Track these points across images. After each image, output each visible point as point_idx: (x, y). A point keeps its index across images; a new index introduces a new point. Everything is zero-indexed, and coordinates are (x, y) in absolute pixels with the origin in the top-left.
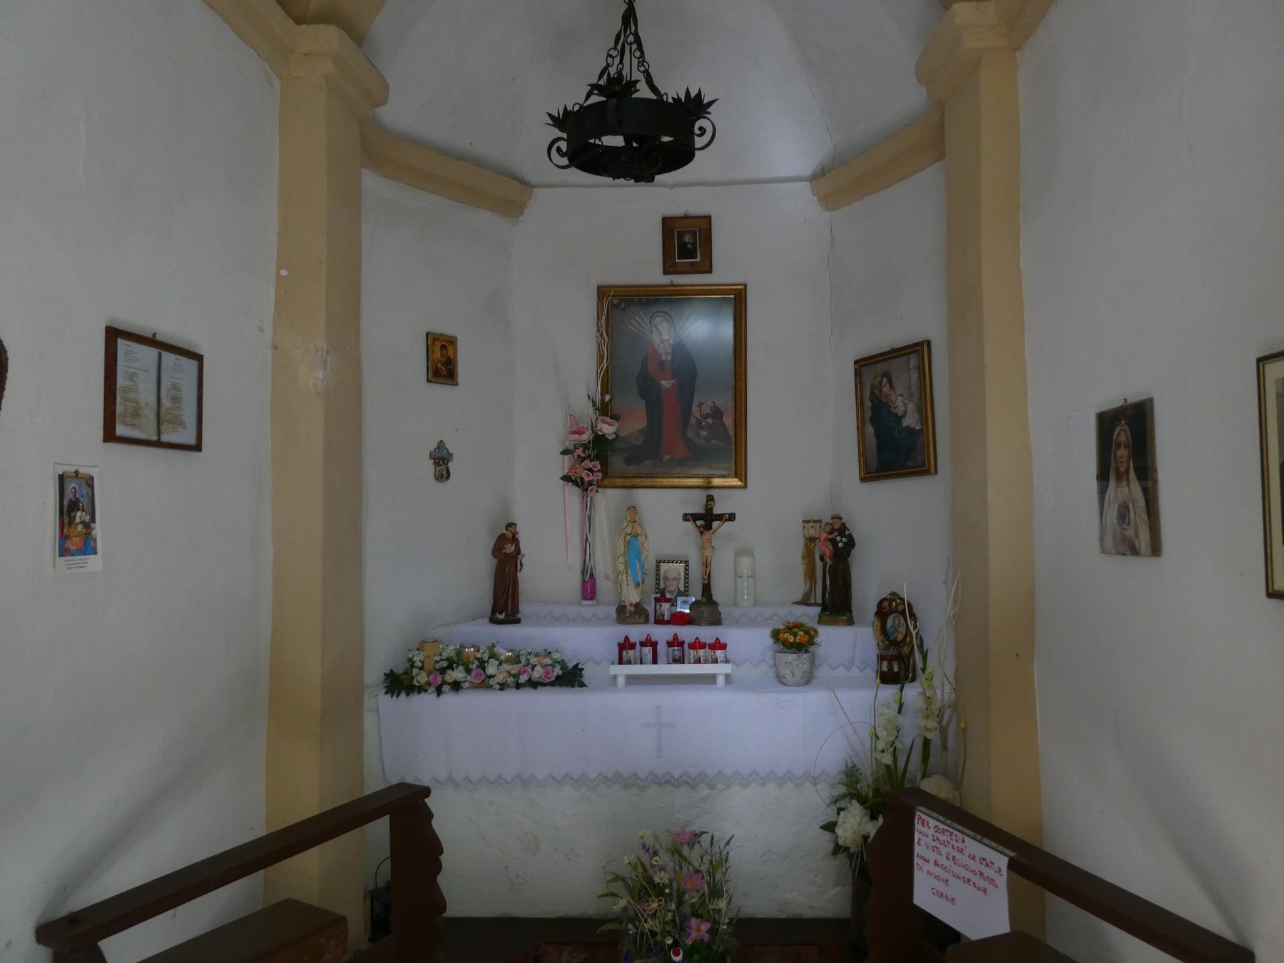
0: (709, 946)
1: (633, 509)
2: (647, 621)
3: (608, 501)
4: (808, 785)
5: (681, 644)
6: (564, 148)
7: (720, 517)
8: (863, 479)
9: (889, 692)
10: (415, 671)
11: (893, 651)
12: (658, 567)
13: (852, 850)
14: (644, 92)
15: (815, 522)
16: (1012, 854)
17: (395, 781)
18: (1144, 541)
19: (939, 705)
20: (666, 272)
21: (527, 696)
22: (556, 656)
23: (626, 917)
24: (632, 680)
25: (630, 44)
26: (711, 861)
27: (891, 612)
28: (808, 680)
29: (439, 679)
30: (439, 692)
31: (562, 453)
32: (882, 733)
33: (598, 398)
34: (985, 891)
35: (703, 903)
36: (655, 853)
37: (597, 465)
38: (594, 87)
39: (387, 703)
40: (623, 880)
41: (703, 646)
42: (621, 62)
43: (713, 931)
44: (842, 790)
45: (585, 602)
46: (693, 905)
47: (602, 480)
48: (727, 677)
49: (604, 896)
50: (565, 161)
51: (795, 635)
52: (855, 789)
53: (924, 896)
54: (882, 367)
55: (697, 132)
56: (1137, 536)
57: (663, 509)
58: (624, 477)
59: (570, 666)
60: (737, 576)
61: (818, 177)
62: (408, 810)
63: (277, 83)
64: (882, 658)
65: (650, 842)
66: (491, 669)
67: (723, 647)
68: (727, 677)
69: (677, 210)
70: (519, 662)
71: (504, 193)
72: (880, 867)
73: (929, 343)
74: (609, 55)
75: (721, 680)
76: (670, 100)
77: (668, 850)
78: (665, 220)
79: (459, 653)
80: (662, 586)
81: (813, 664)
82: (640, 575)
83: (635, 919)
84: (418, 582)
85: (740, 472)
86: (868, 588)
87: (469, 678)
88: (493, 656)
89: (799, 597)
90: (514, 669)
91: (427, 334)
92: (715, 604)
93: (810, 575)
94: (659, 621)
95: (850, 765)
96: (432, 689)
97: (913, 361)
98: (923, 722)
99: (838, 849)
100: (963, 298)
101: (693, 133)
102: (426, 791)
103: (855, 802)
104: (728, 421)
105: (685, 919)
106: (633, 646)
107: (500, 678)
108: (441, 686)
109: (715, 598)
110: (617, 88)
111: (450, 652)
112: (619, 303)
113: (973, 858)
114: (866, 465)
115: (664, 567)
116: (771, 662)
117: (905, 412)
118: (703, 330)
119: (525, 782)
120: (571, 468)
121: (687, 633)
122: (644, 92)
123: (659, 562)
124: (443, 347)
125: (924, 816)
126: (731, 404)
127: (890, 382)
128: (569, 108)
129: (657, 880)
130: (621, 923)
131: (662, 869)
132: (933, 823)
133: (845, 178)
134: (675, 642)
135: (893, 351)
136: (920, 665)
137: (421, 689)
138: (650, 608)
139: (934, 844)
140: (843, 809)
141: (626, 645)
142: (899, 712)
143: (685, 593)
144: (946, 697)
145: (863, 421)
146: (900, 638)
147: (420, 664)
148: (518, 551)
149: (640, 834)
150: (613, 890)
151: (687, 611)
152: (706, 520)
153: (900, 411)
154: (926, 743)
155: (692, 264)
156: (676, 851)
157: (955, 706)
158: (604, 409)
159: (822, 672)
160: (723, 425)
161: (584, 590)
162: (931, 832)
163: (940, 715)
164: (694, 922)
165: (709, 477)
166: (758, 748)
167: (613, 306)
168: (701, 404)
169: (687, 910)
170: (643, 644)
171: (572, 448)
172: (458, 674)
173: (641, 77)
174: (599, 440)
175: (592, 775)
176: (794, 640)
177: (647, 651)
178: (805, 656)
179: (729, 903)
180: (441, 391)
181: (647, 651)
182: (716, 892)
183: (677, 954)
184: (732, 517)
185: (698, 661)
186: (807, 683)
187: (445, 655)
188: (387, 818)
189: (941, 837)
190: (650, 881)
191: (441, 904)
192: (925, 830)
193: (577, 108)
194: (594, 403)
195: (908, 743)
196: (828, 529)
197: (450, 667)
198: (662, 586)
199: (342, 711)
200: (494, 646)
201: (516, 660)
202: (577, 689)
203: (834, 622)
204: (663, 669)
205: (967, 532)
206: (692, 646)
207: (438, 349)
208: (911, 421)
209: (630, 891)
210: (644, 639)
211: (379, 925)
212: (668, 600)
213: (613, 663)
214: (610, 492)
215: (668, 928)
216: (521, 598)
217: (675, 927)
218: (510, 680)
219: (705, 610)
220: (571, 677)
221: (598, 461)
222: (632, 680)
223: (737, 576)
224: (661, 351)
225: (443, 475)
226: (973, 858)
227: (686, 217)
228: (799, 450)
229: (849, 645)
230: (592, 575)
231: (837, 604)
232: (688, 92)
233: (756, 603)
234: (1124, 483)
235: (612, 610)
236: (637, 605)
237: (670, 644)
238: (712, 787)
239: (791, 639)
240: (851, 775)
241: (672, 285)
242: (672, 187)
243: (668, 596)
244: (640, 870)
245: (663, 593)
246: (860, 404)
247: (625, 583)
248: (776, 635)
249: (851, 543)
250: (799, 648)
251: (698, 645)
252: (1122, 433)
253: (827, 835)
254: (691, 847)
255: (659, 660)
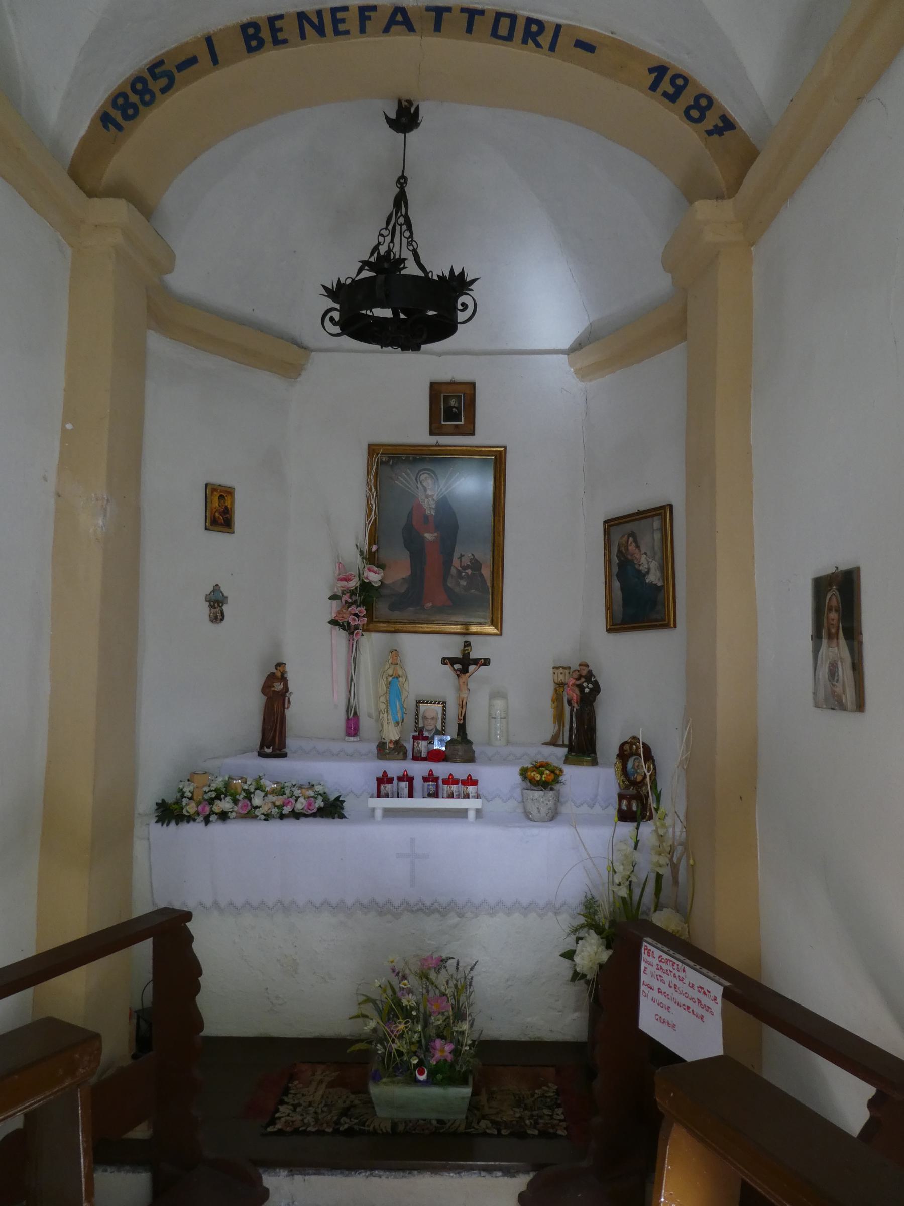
0: (452, 1066)
1: (395, 652)
2: (405, 758)
3: (372, 644)
4: (551, 914)
5: (436, 780)
6: (337, 318)
7: (476, 662)
8: (609, 630)
9: (627, 829)
10: (185, 801)
11: (632, 791)
12: (418, 706)
13: (588, 977)
14: (411, 269)
15: (564, 668)
16: (727, 984)
17: (162, 905)
18: (849, 697)
19: (670, 843)
20: (432, 433)
21: (290, 827)
22: (318, 788)
23: (377, 1037)
24: (389, 813)
25: (401, 225)
26: (456, 986)
27: (631, 755)
28: (553, 816)
29: (208, 809)
30: (207, 821)
31: (330, 599)
32: (619, 868)
33: (365, 549)
34: (702, 1018)
35: (447, 1025)
36: (404, 977)
37: (363, 609)
38: (365, 264)
39: (158, 831)
40: (374, 1002)
41: (456, 782)
42: (392, 241)
43: (456, 1052)
44: (582, 920)
45: (347, 738)
46: (438, 1027)
47: (368, 624)
48: (478, 812)
49: (357, 1016)
50: (337, 329)
51: (542, 774)
52: (593, 919)
53: (648, 1021)
54: (629, 527)
55: (460, 307)
56: (844, 693)
57: (423, 654)
58: (388, 622)
59: (332, 798)
60: (491, 717)
61: (577, 347)
62: (170, 933)
63: (69, 251)
64: (621, 797)
65: (400, 966)
66: (257, 801)
67: (475, 783)
68: (478, 812)
69: (444, 376)
70: (284, 794)
71: (282, 356)
72: (612, 991)
73: (671, 507)
74: (381, 235)
75: (471, 814)
76: (435, 278)
77: (416, 974)
78: (433, 385)
79: (227, 785)
80: (421, 725)
81: (558, 801)
82: (399, 715)
83: (382, 1040)
84: (189, 717)
85: (496, 620)
86: (611, 733)
87: (236, 808)
88: (259, 788)
89: (548, 738)
90: (279, 800)
91: (207, 485)
92: (469, 743)
93: (559, 717)
94: (417, 758)
95: (589, 897)
96: (200, 818)
97: (657, 523)
98: (656, 858)
99: (576, 976)
100: (699, 467)
101: (456, 308)
102: (188, 916)
103: (592, 932)
104: (486, 572)
105: (430, 1040)
106: (390, 781)
107: (264, 809)
108: (209, 816)
109: (469, 738)
110: (386, 265)
111: (219, 783)
112: (387, 460)
113: (692, 986)
114: (612, 617)
115: (423, 707)
116: (520, 799)
117: (649, 569)
118: (469, 486)
119: (286, 908)
120: (339, 612)
121: (442, 769)
122: (411, 269)
123: (418, 702)
124: (221, 497)
125: (649, 947)
126: (489, 557)
127: (635, 541)
128: (342, 282)
129: (405, 1002)
130: (370, 1043)
131: (410, 991)
132: (657, 953)
133: (606, 346)
134: (430, 778)
135: (639, 512)
136: (654, 805)
137: (190, 818)
138: (409, 746)
139: (659, 973)
140: (581, 938)
141: (384, 780)
142: (635, 848)
143: (442, 732)
144: (678, 833)
145: (610, 576)
146: (639, 779)
147: (190, 795)
148: (286, 689)
149: (391, 959)
150: (365, 1012)
151: (444, 749)
152: (463, 664)
153: (643, 568)
154: (659, 877)
155: (457, 426)
156: (424, 976)
157: (685, 845)
158: (371, 559)
159: (567, 809)
160: (482, 576)
161: (348, 727)
162: (656, 961)
163: (671, 852)
164: (439, 1043)
165: (467, 624)
166: (504, 882)
167: (382, 463)
168: (462, 556)
169: (432, 1032)
170: (400, 779)
171: (339, 594)
172: (225, 804)
173: (407, 254)
174: (365, 587)
175: (349, 901)
176: (541, 779)
177: (404, 785)
178: (551, 793)
179: (471, 1025)
180: (218, 538)
181: (404, 785)
182: (460, 1015)
183: (421, 1074)
184: (487, 662)
185: (451, 796)
186: (552, 818)
187: (214, 786)
188: (150, 940)
189: (665, 967)
190: (398, 1003)
191: (199, 1023)
192: (650, 959)
193: (349, 281)
194: (362, 553)
195: (643, 877)
196: (576, 675)
197: (218, 798)
198: (421, 725)
199: (111, 838)
200: (260, 778)
201: (281, 792)
202: (337, 820)
203: (578, 763)
204: (419, 802)
205: (698, 682)
206: (445, 782)
207: (216, 499)
208: (653, 578)
209: (380, 1012)
210: (401, 774)
211: (142, 1043)
212: (426, 738)
213: (372, 797)
214: (374, 636)
215: (414, 1048)
216: (289, 733)
217: (420, 1047)
218: (275, 811)
219: (460, 748)
220: (332, 809)
221: (364, 607)
222: (389, 813)
223: (491, 717)
224: (426, 506)
225: (218, 617)
226: (692, 986)
227: (452, 383)
228: (552, 599)
229: (592, 784)
230: (355, 713)
231: (582, 745)
232: (452, 271)
233: (508, 743)
234: (835, 641)
235: (373, 747)
236: (397, 742)
237: (425, 780)
238: (461, 915)
239: (538, 777)
240: (590, 906)
241: (438, 445)
242: (440, 355)
243: (426, 734)
244: (389, 992)
245: (421, 731)
246: (608, 562)
247: (386, 721)
248: (524, 773)
249: (596, 689)
250: (545, 786)
251: (451, 781)
252: (833, 597)
253: (566, 963)
254: (438, 972)
255: (415, 794)
